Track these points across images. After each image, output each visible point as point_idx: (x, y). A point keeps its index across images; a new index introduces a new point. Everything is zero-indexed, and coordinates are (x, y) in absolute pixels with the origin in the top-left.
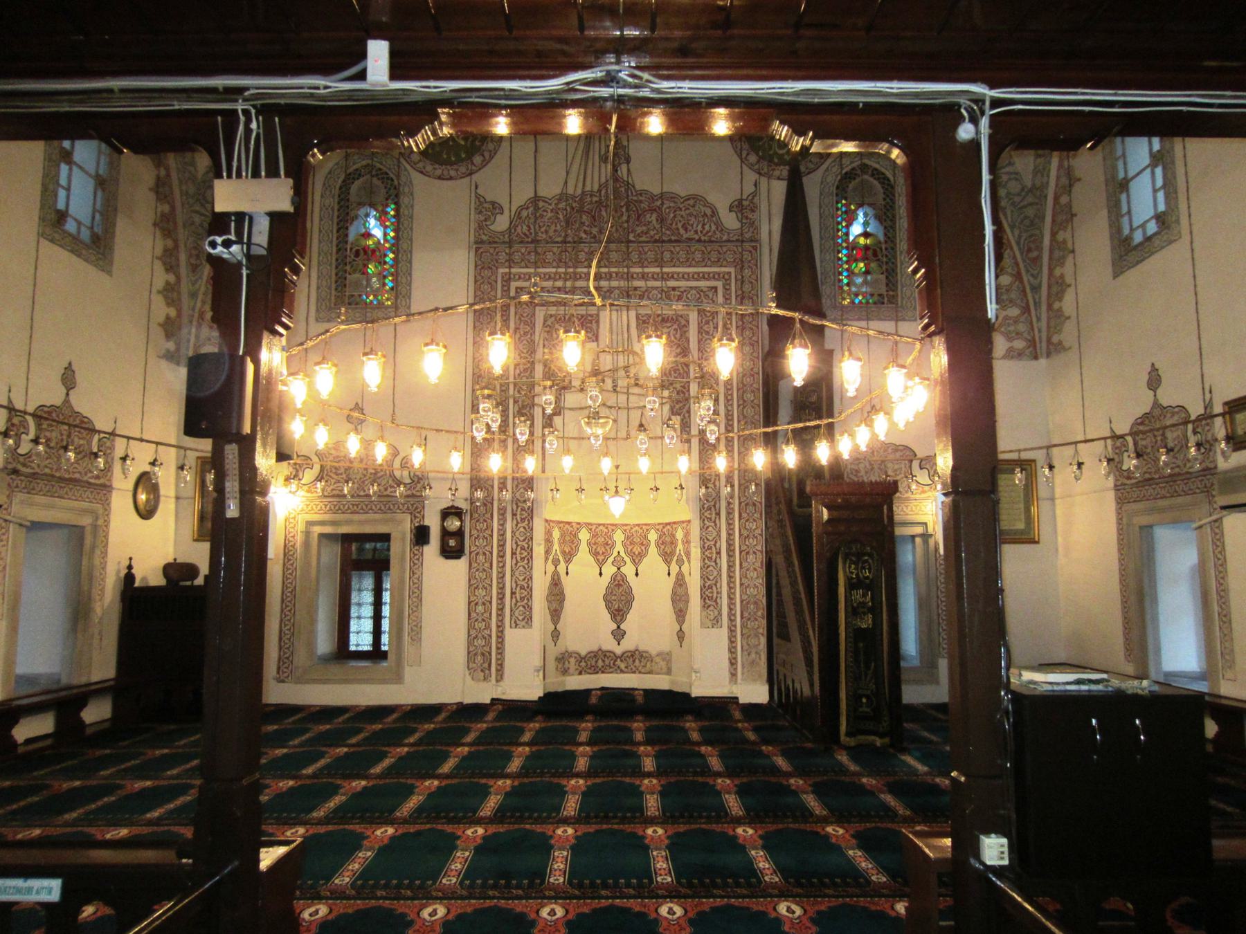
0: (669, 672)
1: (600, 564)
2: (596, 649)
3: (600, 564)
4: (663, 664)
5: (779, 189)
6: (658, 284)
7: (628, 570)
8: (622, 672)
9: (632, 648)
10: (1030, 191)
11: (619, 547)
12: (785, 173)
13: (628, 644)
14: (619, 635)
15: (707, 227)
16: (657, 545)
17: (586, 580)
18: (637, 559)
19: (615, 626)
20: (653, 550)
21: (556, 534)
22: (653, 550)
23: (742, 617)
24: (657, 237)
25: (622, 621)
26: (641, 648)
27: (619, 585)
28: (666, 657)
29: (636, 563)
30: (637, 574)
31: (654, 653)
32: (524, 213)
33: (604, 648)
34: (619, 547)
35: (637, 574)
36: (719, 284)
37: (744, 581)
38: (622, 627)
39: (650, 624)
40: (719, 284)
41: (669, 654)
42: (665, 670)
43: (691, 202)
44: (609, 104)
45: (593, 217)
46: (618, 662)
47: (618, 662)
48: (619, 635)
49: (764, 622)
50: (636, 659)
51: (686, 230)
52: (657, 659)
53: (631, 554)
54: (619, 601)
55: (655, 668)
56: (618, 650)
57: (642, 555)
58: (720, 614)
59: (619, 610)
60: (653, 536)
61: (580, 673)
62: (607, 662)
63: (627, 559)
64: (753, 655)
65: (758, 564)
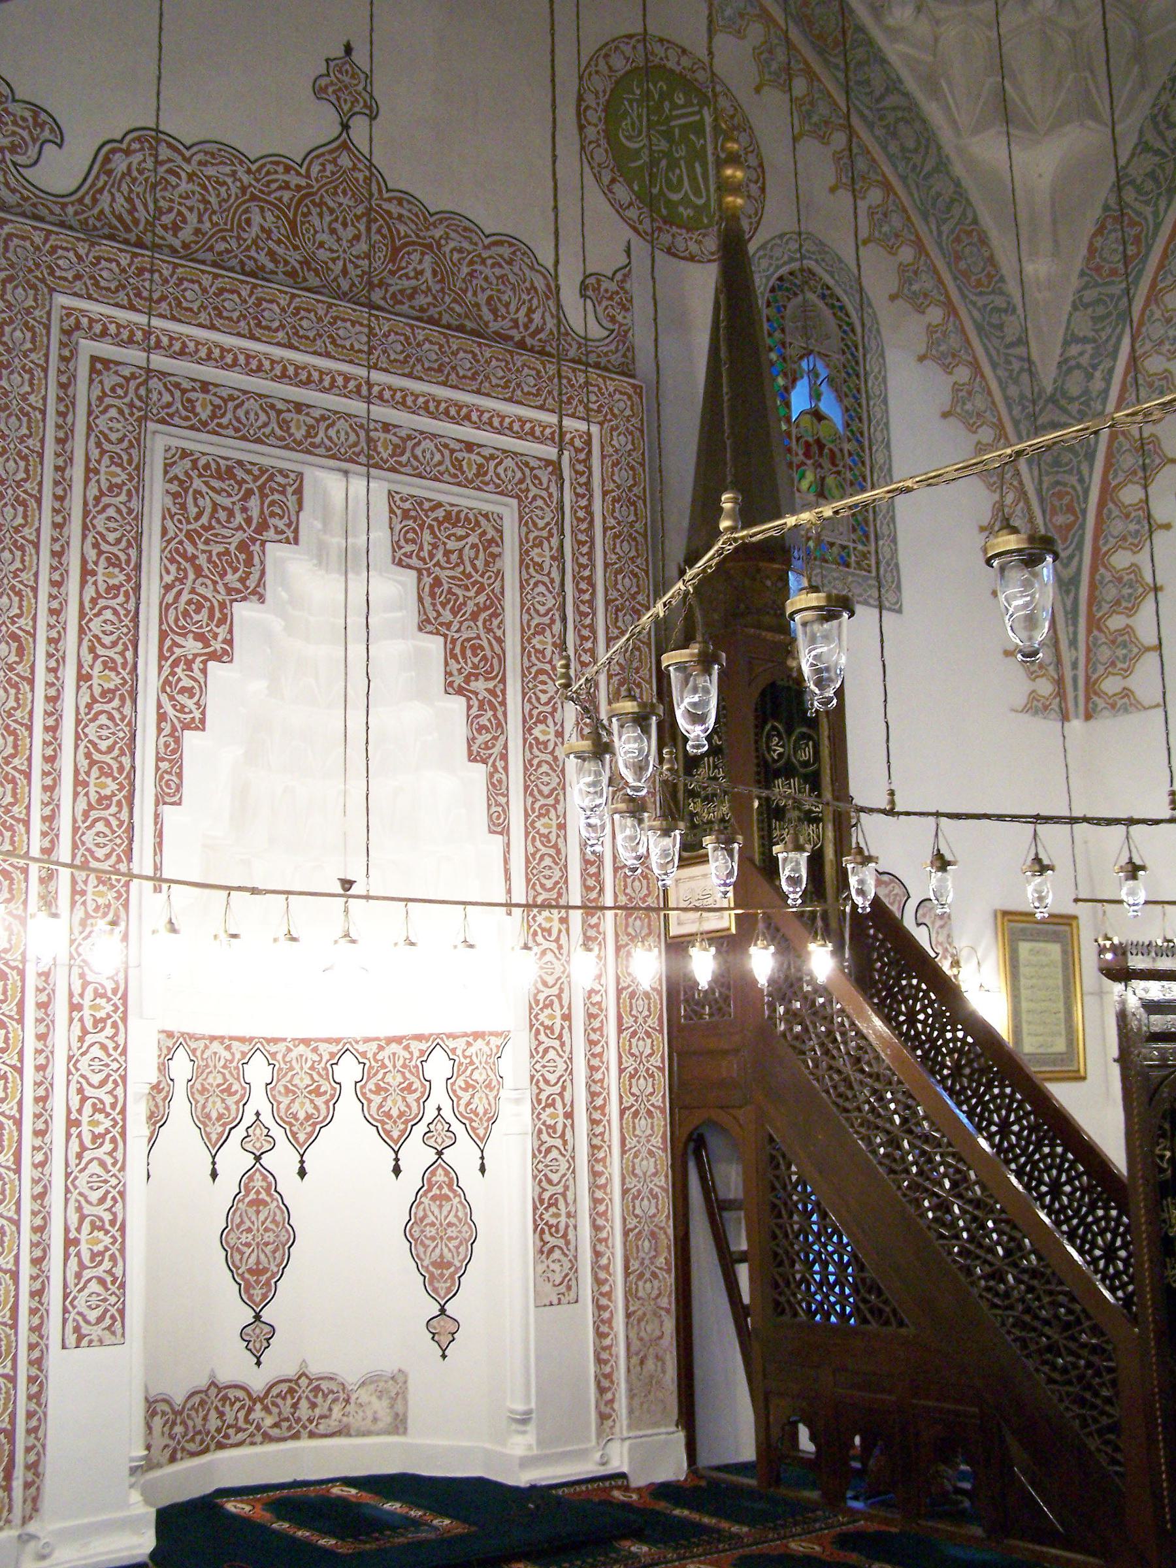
0: (399, 1425)
1: (215, 1146)
2: (203, 1383)
3: (215, 1146)
4: (380, 1407)
5: (700, 285)
6: (356, 406)
7: (281, 1160)
8: (268, 1438)
9: (291, 1371)
10: (1052, 400)
11: (259, 1102)
12: (711, 244)
13: (281, 1361)
14: (258, 1337)
15: (537, 317)
16: (362, 1098)
17: (175, 1192)
18: (306, 1131)
19: (249, 1316)
20: (348, 1106)
21: (181, 1068)
22: (348, 1106)
23: (627, 1273)
24: (433, 312)
25: (266, 1300)
26: (314, 1369)
27: (258, 1203)
28: (393, 1387)
29: (302, 1149)
30: (302, 1173)
31: (351, 1378)
32: (120, 164)
33: (224, 1378)
34: (259, 1102)
35: (302, 1173)
36: (88, 347)
37: (631, 1182)
38: (266, 1315)
39: (348, 1298)
40: (88, 347)
41: (399, 1379)
42: (386, 1419)
43: (506, 251)
44: (877, 133)
45: (293, 224)
46: (258, 1413)
47: (258, 1413)
48: (258, 1337)
49: (670, 1279)
50: (300, 1403)
51: (494, 312)
52: (364, 1395)
53: (288, 1122)
54: (258, 1250)
55: (355, 1421)
56: (257, 1381)
57: (318, 1124)
58: (574, 1268)
59: (257, 1271)
60: (348, 1071)
61: (173, 1459)
62: (229, 1418)
63: (277, 1132)
64: (650, 1364)
65: (657, 1141)
